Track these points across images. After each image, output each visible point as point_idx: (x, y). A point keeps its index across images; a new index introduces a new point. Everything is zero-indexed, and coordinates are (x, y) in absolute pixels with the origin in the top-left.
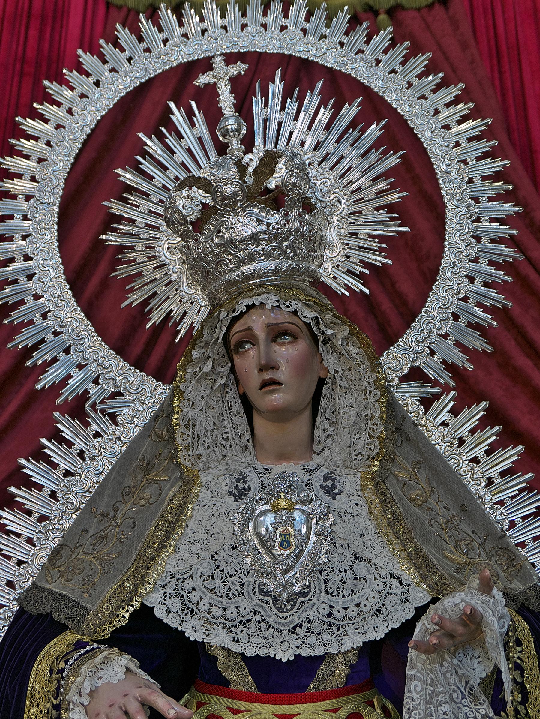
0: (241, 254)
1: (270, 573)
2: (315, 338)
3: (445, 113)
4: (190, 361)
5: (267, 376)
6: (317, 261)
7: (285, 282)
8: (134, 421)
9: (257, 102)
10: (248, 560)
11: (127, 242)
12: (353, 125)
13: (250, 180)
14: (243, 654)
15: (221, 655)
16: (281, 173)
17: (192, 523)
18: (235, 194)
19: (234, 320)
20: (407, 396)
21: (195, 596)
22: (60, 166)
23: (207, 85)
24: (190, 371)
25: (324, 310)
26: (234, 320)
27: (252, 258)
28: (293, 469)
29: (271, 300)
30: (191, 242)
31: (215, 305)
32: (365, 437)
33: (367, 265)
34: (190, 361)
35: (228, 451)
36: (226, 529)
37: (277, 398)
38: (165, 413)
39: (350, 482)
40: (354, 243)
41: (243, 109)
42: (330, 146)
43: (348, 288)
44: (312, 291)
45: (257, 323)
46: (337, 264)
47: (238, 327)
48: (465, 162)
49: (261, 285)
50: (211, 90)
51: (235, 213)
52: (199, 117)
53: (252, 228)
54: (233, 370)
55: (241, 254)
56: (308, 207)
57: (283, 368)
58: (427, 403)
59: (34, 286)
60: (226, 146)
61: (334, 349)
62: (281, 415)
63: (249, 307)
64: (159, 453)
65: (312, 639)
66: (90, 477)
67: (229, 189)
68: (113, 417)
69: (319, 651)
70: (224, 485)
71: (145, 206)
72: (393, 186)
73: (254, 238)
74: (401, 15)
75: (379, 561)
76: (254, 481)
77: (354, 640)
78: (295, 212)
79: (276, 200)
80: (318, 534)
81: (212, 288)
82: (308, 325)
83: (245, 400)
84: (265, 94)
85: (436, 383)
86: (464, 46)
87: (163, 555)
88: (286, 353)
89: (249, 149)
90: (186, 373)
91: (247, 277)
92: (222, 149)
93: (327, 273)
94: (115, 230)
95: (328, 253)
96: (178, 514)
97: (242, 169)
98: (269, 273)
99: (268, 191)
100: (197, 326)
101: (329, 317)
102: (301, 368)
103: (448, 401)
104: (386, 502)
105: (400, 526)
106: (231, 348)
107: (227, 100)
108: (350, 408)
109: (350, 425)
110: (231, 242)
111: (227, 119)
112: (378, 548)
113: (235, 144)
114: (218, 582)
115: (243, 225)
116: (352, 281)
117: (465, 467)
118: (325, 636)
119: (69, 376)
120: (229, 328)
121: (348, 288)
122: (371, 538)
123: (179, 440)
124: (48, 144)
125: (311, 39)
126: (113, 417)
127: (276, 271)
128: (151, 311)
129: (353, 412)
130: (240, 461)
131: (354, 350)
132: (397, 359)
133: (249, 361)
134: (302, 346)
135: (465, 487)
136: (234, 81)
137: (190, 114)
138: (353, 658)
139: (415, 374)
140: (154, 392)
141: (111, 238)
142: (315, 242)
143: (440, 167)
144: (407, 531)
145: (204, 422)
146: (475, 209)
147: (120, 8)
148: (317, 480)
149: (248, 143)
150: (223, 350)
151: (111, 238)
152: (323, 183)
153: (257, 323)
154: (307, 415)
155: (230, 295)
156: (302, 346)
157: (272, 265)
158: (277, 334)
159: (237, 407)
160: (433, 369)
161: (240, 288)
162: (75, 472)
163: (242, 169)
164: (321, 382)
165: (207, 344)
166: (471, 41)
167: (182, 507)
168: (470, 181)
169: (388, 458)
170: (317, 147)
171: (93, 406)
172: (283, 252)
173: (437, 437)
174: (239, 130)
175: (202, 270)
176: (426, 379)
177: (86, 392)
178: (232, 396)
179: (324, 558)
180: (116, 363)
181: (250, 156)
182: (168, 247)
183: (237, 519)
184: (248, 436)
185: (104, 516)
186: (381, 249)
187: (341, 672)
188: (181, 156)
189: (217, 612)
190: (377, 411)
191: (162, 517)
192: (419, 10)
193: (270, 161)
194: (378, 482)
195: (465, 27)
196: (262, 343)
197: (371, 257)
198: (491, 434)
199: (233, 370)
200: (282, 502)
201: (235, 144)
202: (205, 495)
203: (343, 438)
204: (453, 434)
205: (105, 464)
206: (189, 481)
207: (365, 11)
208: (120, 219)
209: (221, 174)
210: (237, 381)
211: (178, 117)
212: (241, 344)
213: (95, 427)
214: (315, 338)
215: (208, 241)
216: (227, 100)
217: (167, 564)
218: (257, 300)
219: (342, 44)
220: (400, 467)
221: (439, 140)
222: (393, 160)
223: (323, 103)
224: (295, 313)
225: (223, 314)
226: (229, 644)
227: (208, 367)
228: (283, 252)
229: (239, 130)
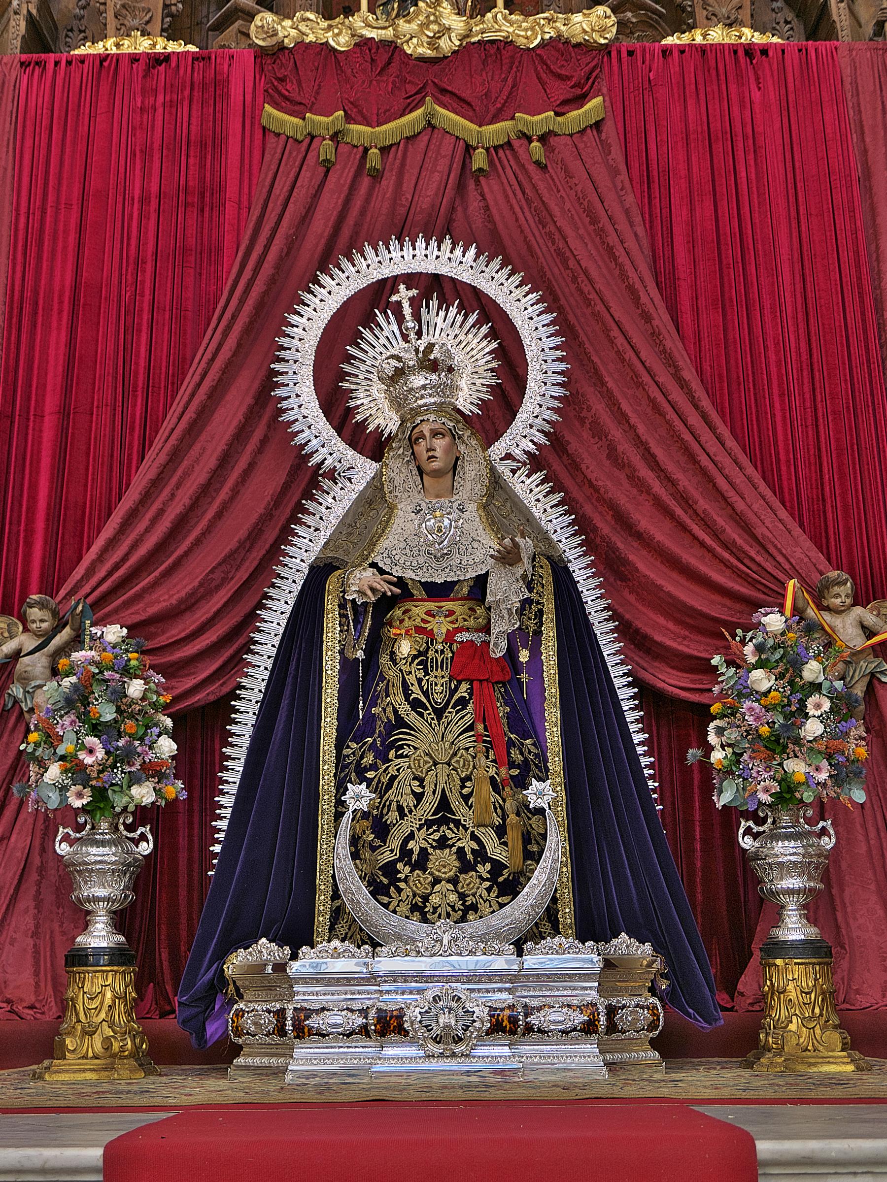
0: (417, 395)
1: (431, 545)
2: (454, 436)
3: (530, 309)
4: (391, 448)
5: (430, 454)
6: (455, 398)
7: (440, 408)
8: (360, 483)
9: (423, 311)
10: (422, 540)
11: (353, 387)
12: (473, 326)
13: (420, 355)
14: (420, 581)
15: (410, 583)
16: (435, 354)
17: (395, 526)
18: (414, 365)
19: (414, 428)
20: (503, 468)
21: (397, 557)
22: (312, 343)
23: (396, 302)
24: (391, 454)
25: (458, 422)
26: (414, 428)
27: (422, 397)
28: (444, 501)
29: (432, 417)
30: (392, 389)
31: (403, 422)
32: (479, 485)
33: (480, 399)
34: (391, 448)
35: (411, 494)
36: (411, 528)
37: (435, 465)
38: (379, 475)
39: (472, 507)
40: (474, 388)
41: (417, 317)
42: (462, 337)
43: (471, 412)
44: (453, 413)
45: (426, 429)
46: (466, 397)
47: (416, 431)
48: (540, 339)
49: (427, 410)
50: (399, 303)
51: (414, 375)
52: (392, 318)
53: (422, 382)
54: (413, 453)
55: (417, 395)
56: (450, 370)
57: (438, 450)
58: (514, 472)
59: (304, 411)
60: (408, 336)
61: (464, 442)
62: (437, 474)
63: (421, 421)
64: (375, 499)
65: (452, 574)
66: (339, 510)
67: (411, 363)
68: (350, 480)
69: (456, 579)
70: (409, 509)
71: (363, 367)
72: (493, 359)
73: (424, 387)
74: (553, 141)
75: (484, 542)
76: (424, 506)
77: (471, 574)
78: (444, 374)
79: (433, 366)
80: (455, 528)
81: (402, 412)
82: (450, 429)
83: (419, 468)
84: (428, 306)
85: (519, 461)
86: (614, 172)
87: (382, 539)
88: (440, 444)
89: (419, 338)
90: (389, 456)
91: (421, 406)
92: (405, 338)
93: (461, 404)
94: (347, 381)
95: (461, 394)
96: (388, 522)
97: (417, 351)
98: (431, 404)
99: (429, 360)
100: (394, 432)
101: (460, 425)
102: (448, 451)
103: (524, 471)
104: (488, 514)
105: (495, 524)
106: (412, 442)
107: (407, 310)
108: (472, 475)
109: (471, 481)
110: (412, 389)
111: (407, 322)
112: (484, 536)
113: (412, 336)
114: (408, 551)
115: (418, 381)
116: (473, 408)
117: (533, 503)
118: (458, 573)
119: (325, 459)
120: (412, 432)
121: (471, 412)
122: (481, 531)
123: (386, 489)
124: (304, 329)
125: (454, 264)
126: (350, 480)
127: (434, 403)
128: (369, 424)
129: (473, 473)
130: (417, 498)
131: (474, 442)
132: (498, 449)
133: (421, 448)
134: (447, 439)
135: (532, 513)
136: (412, 300)
137: (387, 317)
138: (471, 583)
139: (508, 456)
140: (365, 469)
141: (346, 385)
142: (454, 388)
143: (526, 341)
144: (498, 529)
145: (398, 480)
146: (544, 367)
147: (278, 135)
148: (455, 505)
149: (419, 334)
150: (408, 443)
151: (346, 385)
152: (459, 357)
153: (426, 429)
154: (451, 473)
155: (409, 417)
156: (447, 439)
157: (432, 400)
158: (435, 434)
159: (415, 472)
160: (517, 453)
161: (415, 412)
162: (332, 508)
163: (417, 351)
164: (457, 459)
165: (400, 440)
166: (623, 167)
167: (389, 519)
168: (543, 350)
169: (490, 496)
170: (456, 336)
171: (339, 474)
172: (438, 394)
173: (518, 488)
174: (414, 328)
175: (397, 403)
176: (514, 459)
177: (335, 467)
178: (412, 466)
179: (458, 538)
180: (351, 453)
181: (420, 341)
182: (378, 389)
183: (416, 522)
184: (421, 486)
185: (350, 525)
186: (487, 391)
187: (465, 590)
188: (383, 341)
189: (408, 564)
190: (485, 472)
191: (380, 523)
192: (571, 135)
193: (430, 347)
194: (485, 507)
195: (617, 153)
196: (428, 439)
197: (482, 396)
198: (547, 487)
199: (413, 453)
200: (438, 514)
201: (412, 336)
202: (400, 513)
203: (468, 486)
204: (528, 489)
205: (347, 504)
206: (392, 508)
207: (519, 138)
208: (349, 374)
209: (407, 356)
210: (415, 457)
211: (380, 319)
212: (417, 439)
213: (340, 485)
214: (454, 436)
215: (400, 389)
216: (407, 310)
217: (384, 543)
218: (425, 418)
219: (472, 267)
220: (497, 500)
221: (526, 326)
222: (494, 345)
223: (459, 312)
224: (444, 423)
225: (409, 425)
226: (414, 577)
227: (401, 450)
228: (438, 394)
229: (414, 328)
